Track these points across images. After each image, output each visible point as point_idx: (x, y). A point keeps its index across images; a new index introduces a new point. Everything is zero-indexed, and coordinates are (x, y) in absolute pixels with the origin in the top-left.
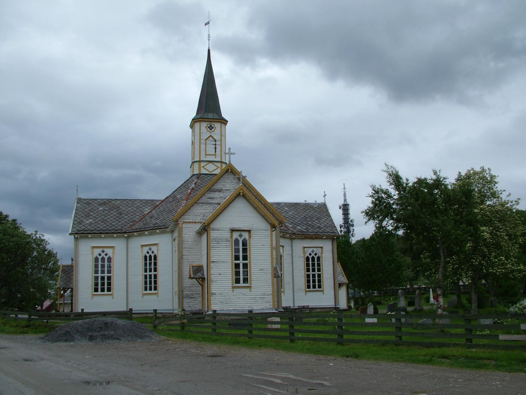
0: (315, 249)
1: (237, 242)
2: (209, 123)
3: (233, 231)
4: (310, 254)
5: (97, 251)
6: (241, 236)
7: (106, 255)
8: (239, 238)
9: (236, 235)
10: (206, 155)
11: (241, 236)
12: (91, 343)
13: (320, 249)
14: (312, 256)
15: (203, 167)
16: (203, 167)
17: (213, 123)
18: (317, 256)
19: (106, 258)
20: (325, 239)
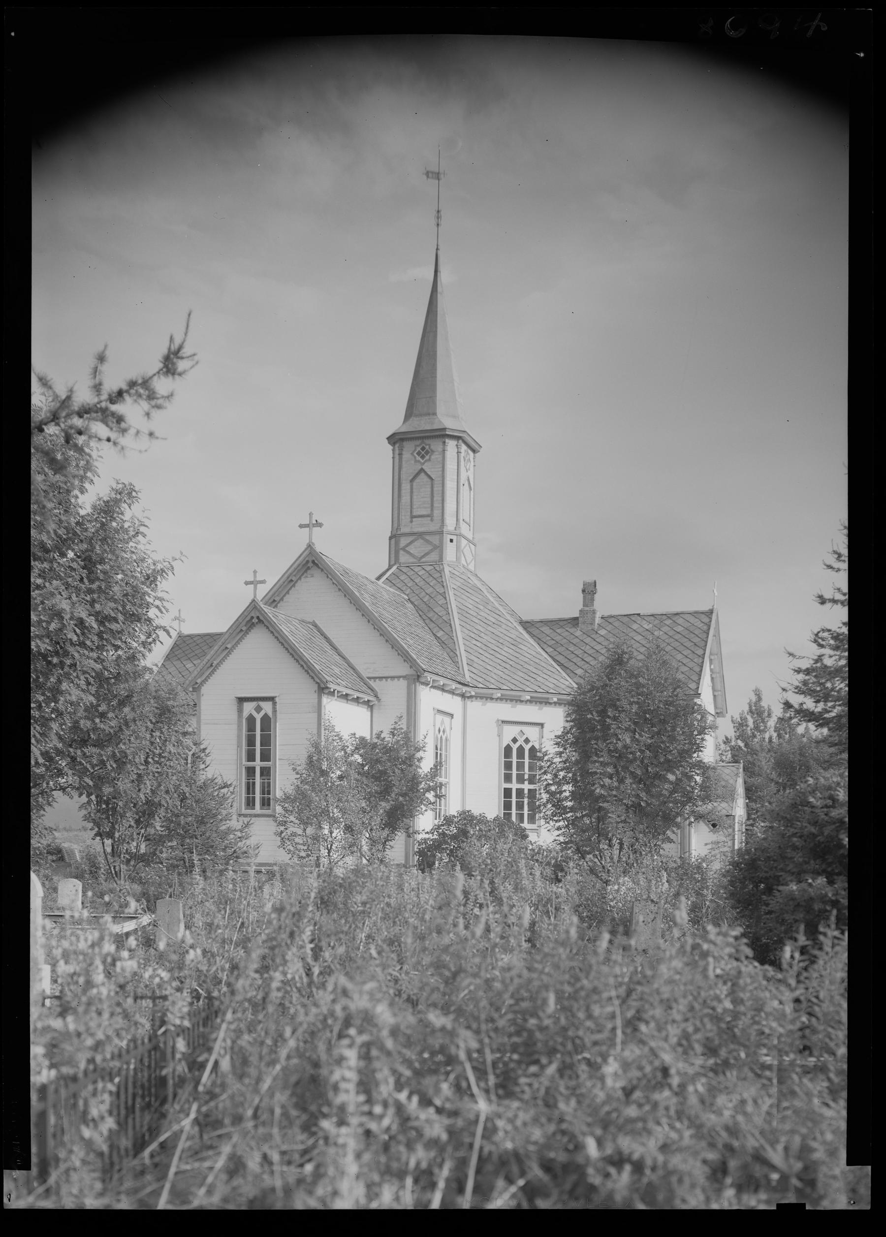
0: (525, 729)
1: (251, 720)
2: (418, 442)
3: (241, 700)
4: (515, 740)
5: (511, 732)
6: (258, 709)
7: (527, 741)
8: (255, 714)
9: (249, 708)
10: (413, 517)
11: (258, 709)
12: (65, 845)
13: (537, 729)
14: (518, 744)
15: (404, 549)
16: (404, 549)
17: (427, 441)
18: (518, 744)
19: (527, 748)
20: (555, 703)
